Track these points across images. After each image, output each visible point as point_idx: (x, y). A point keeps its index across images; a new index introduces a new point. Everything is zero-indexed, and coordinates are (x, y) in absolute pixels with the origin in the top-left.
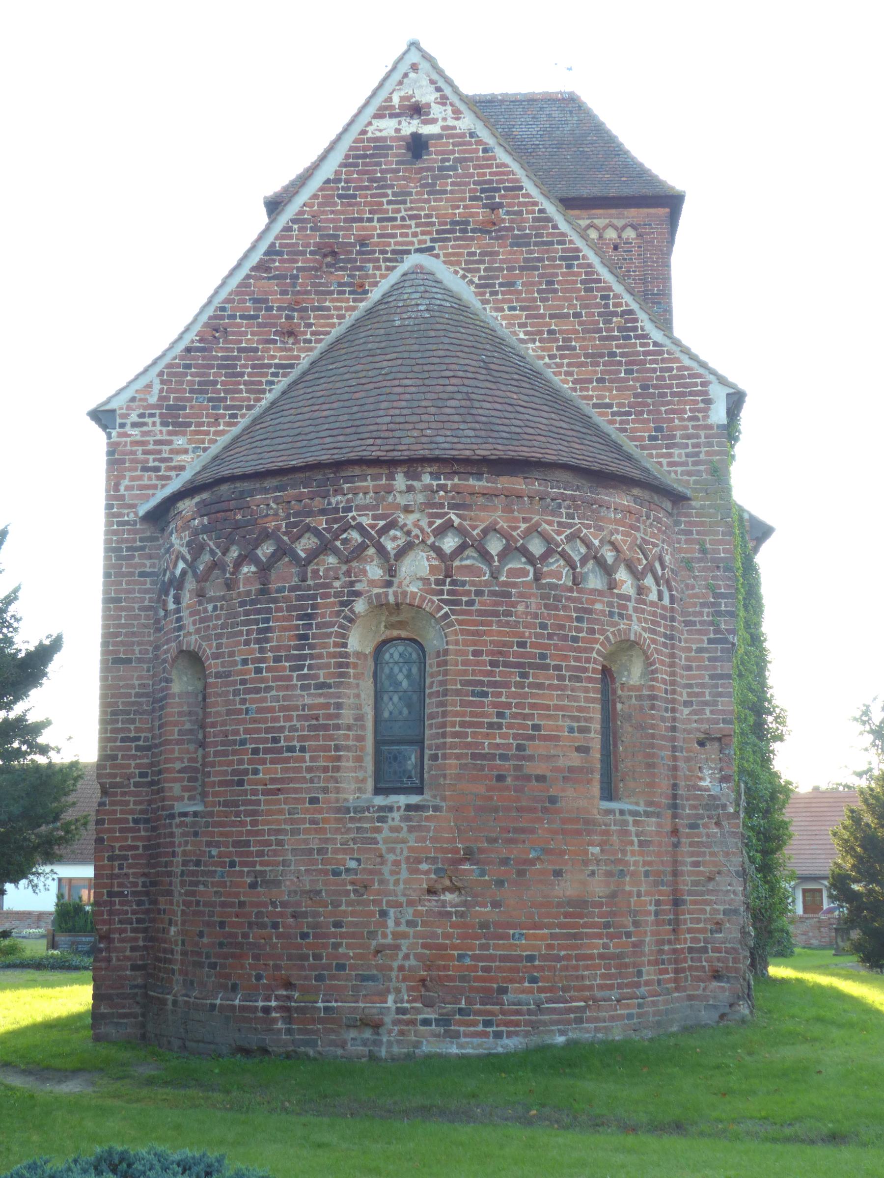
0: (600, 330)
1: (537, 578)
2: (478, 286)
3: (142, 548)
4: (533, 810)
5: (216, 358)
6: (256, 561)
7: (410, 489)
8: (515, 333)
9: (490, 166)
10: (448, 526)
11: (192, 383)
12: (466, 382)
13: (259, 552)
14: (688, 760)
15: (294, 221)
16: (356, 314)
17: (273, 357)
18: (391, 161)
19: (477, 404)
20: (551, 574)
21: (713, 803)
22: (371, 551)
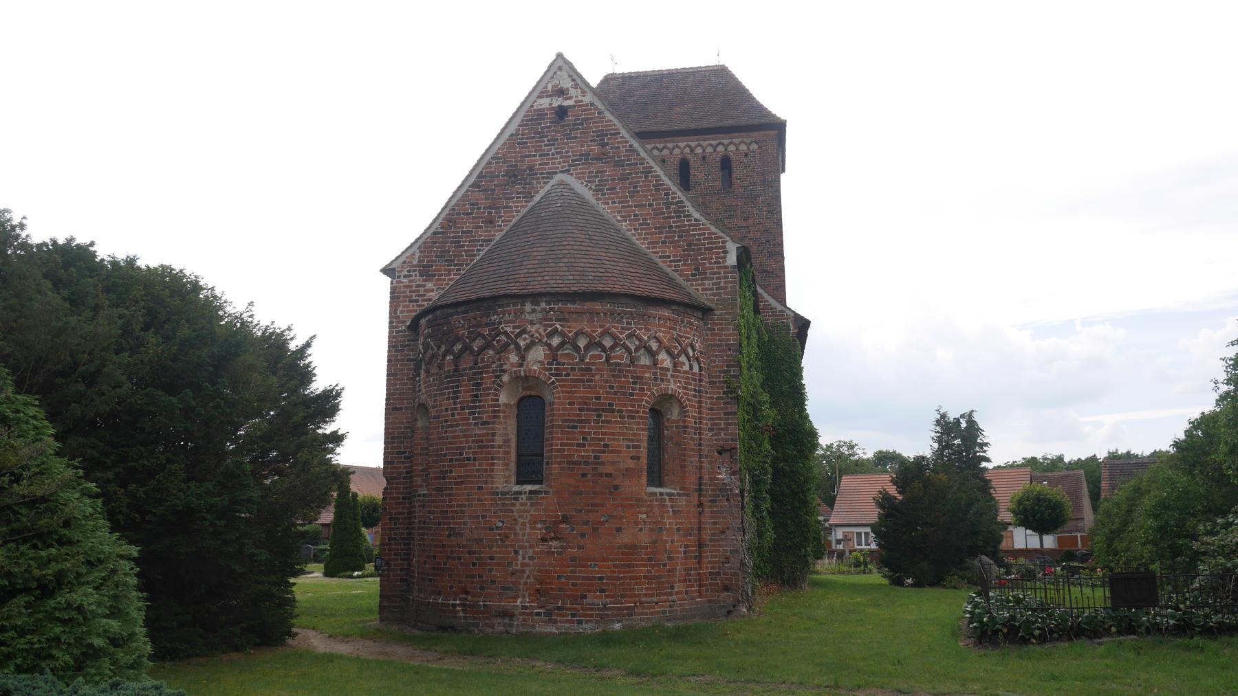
4: (604, 493)
7: (533, 311)
14: (711, 462)
16: (526, 209)
18: (546, 123)
20: (616, 357)
21: (724, 489)
22: (512, 347)
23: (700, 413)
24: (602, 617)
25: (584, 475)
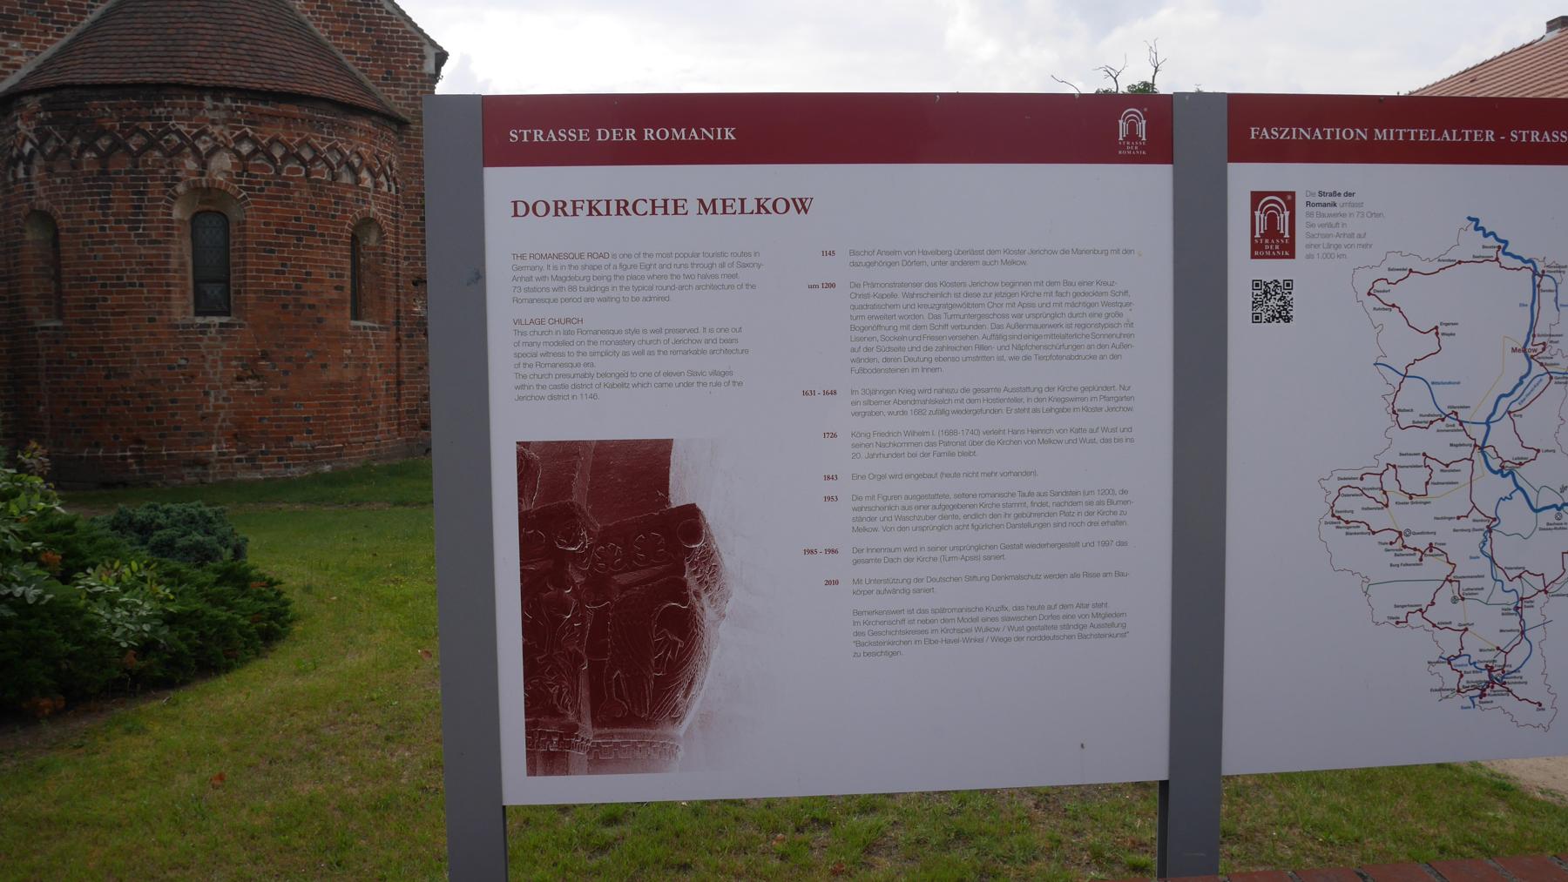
1: (308, 174)
6: (97, 150)
13: (99, 144)
14: (406, 294)
20: (317, 173)
22: (188, 150)
24: (310, 459)
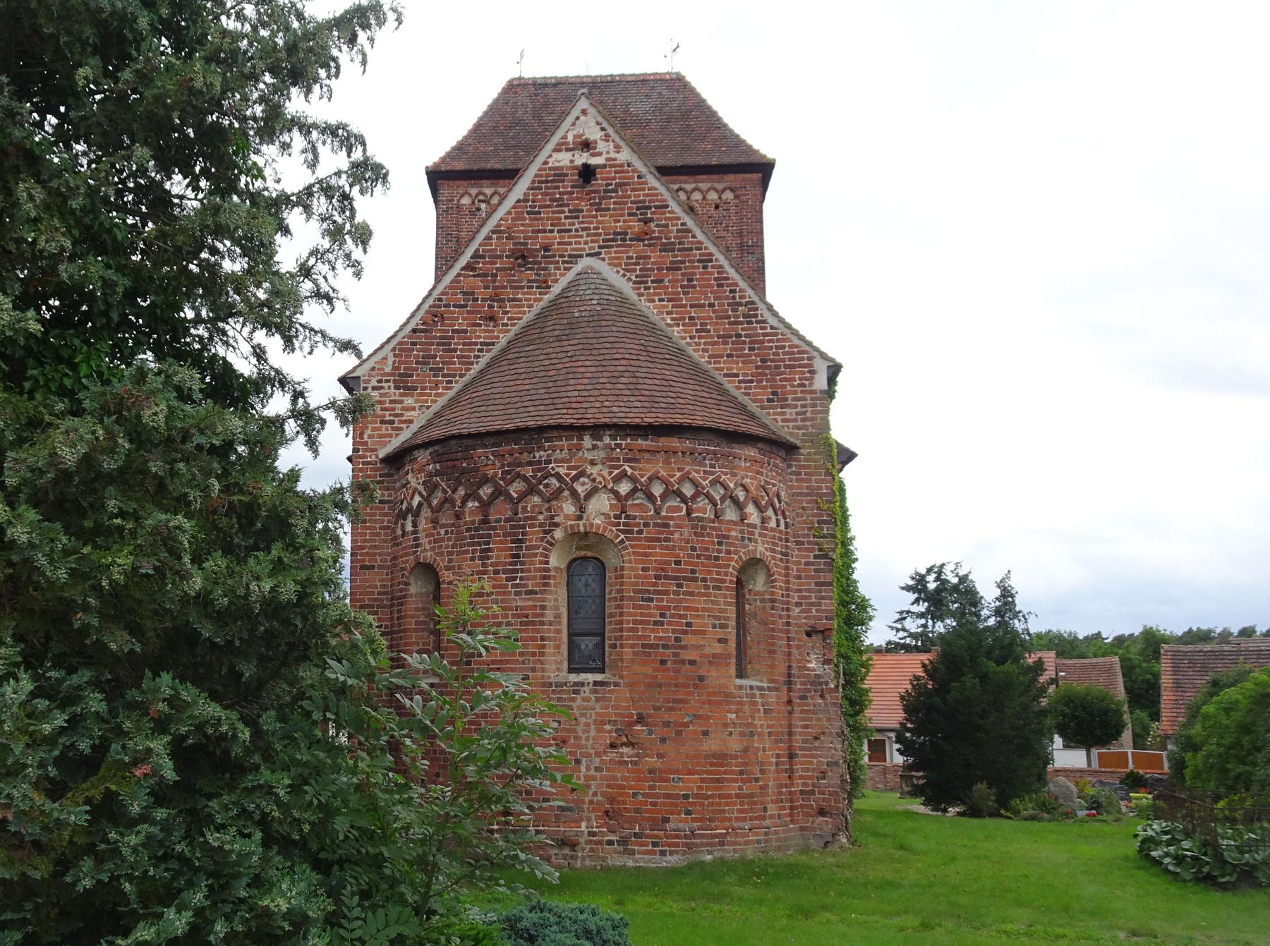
0: (729, 317)
1: (689, 513)
2: (635, 283)
3: (382, 482)
5: (435, 337)
6: (479, 499)
7: (595, 447)
8: (664, 319)
9: (644, 189)
10: (624, 475)
11: (418, 356)
12: (632, 363)
13: (481, 492)
14: (798, 647)
15: (493, 232)
16: (542, 304)
17: (479, 337)
18: (567, 186)
19: (641, 381)
20: (698, 510)
21: (817, 681)
22: (566, 493)
23: (788, 582)
25: (663, 662)
